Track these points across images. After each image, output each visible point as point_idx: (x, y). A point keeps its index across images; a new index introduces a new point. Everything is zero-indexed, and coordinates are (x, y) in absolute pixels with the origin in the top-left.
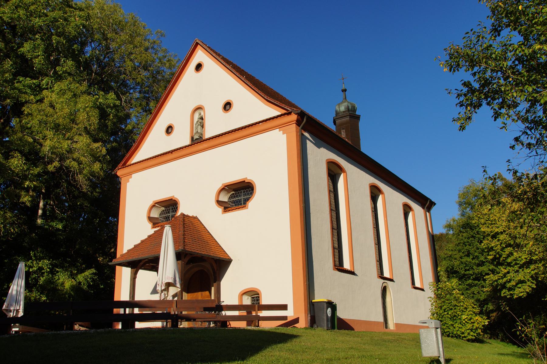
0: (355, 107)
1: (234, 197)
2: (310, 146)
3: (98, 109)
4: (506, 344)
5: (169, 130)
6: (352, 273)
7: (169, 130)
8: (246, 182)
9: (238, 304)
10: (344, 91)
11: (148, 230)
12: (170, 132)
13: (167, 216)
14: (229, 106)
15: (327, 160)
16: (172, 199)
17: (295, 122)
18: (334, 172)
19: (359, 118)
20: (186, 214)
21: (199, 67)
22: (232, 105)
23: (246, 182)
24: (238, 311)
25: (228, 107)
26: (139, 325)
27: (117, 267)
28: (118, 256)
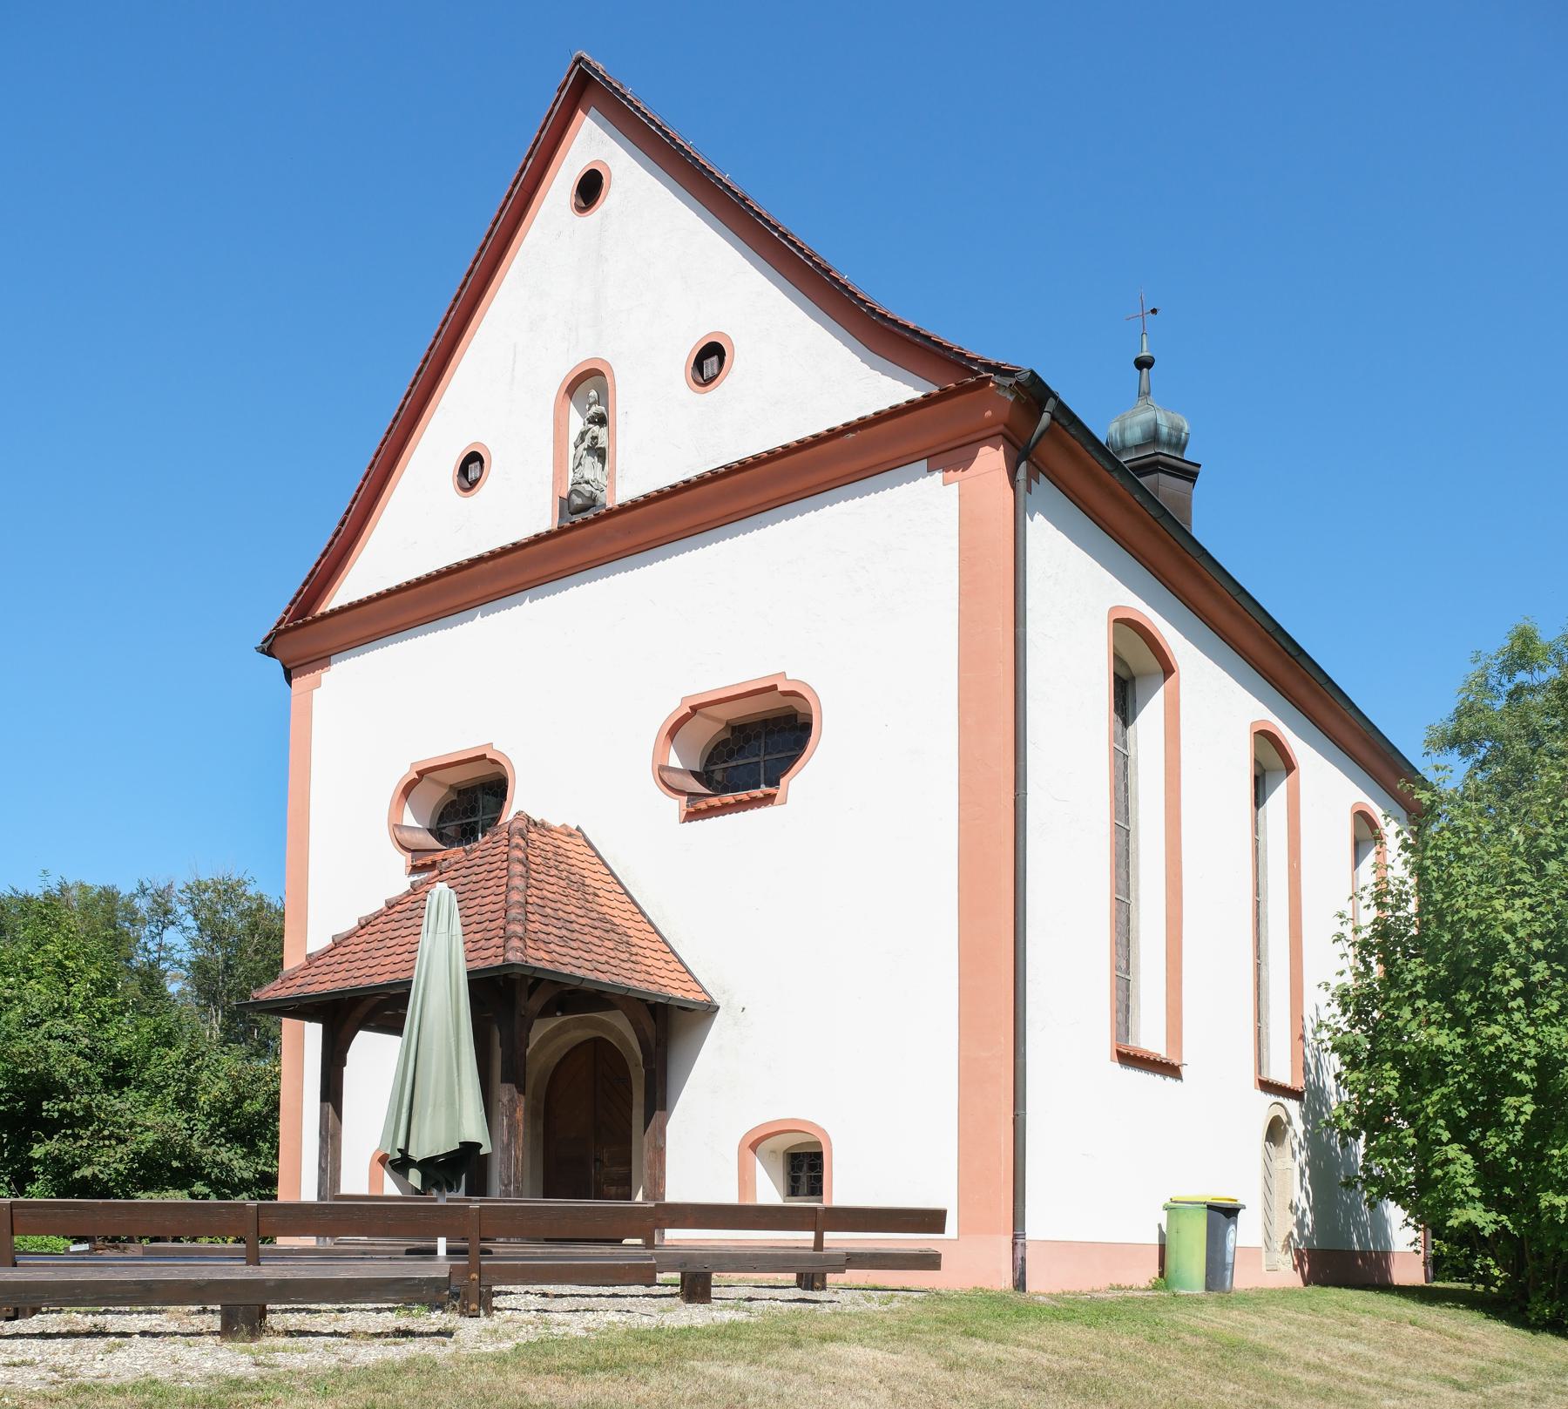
0: (1181, 430)
1: (731, 755)
2: (1141, 480)
3: (242, 1180)
4: (1530, 1334)
5: (471, 468)
6: (1170, 1070)
7: (471, 468)
8: (780, 689)
9: (365, 1191)
10: (1143, 364)
11: (395, 877)
12: (477, 481)
13: (468, 824)
14: (715, 359)
15: (1113, 609)
16: (483, 757)
17: (1001, 428)
18: (1129, 668)
19: (1196, 475)
20: (537, 819)
21: (590, 188)
22: (727, 358)
23: (780, 689)
24: (302, 1200)
25: (711, 364)
26: (639, 1241)
27: (288, 1024)
28: (292, 960)
